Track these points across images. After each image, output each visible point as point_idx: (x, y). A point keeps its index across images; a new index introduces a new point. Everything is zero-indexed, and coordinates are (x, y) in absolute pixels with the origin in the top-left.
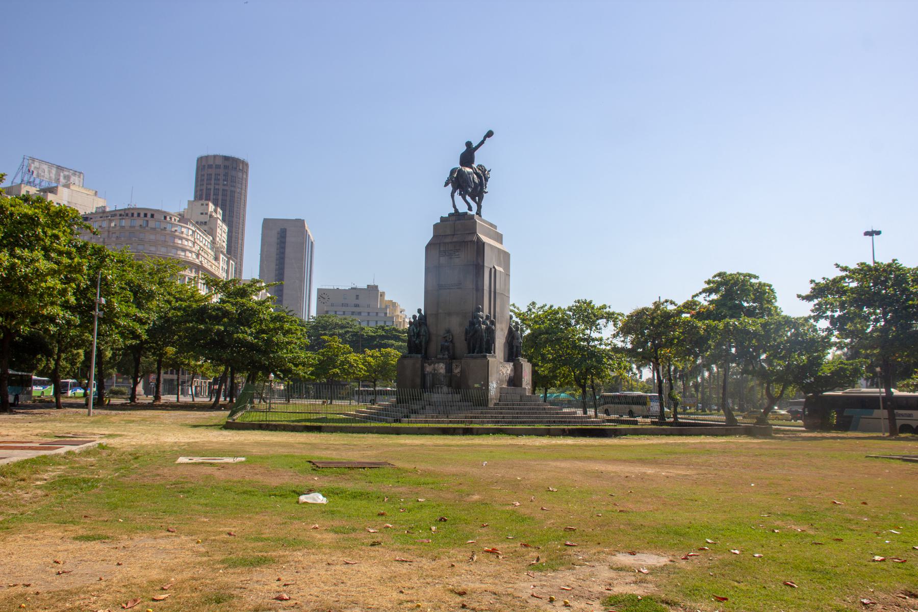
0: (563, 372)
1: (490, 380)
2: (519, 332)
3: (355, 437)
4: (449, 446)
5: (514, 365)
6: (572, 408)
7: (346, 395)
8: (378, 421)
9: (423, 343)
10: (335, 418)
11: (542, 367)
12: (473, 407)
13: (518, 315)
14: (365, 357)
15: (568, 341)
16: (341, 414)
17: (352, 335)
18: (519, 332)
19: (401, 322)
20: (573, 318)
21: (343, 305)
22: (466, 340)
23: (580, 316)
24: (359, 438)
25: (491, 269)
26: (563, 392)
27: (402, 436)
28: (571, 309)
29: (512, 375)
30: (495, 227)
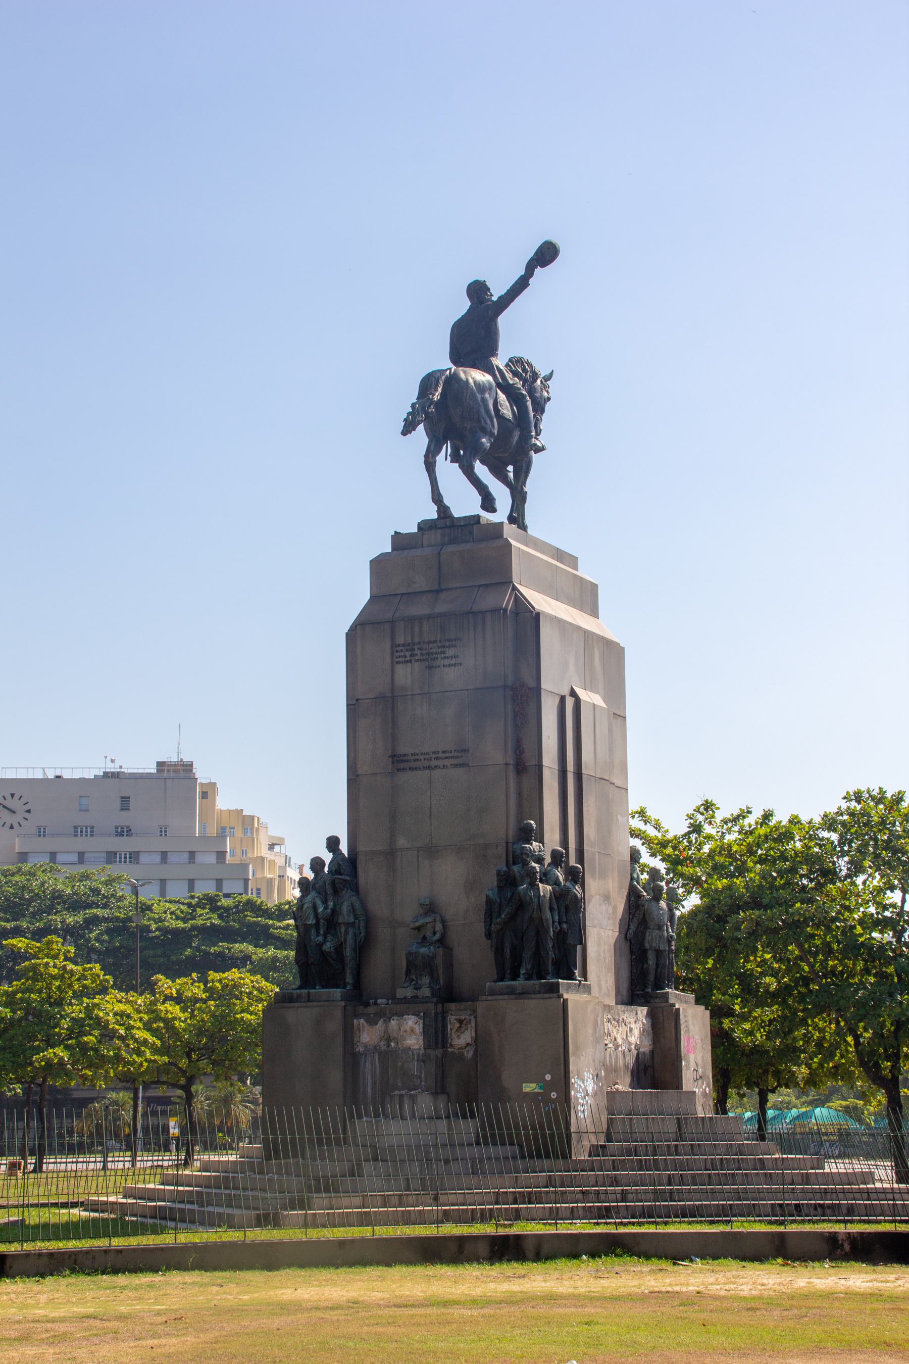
0: (817, 1035)
1: (572, 1067)
2: (663, 904)
3: (123, 1288)
4: (446, 1304)
5: (651, 1015)
6: (857, 1156)
7: (91, 1136)
8: (202, 1224)
9: (348, 952)
10: (54, 1220)
11: (744, 1018)
12: (520, 1162)
13: (659, 846)
14: (153, 1003)
15: (829, 929)
16: (74, 1205)
17: (108, 931)
18: (663, 904)
19: (270, 881)
20: (843, 854)
21: (77, 831)
22: (488, 935)
23: (865, 845)
24: (136, 1288)
25: (563, 699)
26: (821, 1103)
27: (283, 1272)
28: (835, 821)
29: (646, 1048)
30: (573, 561)
